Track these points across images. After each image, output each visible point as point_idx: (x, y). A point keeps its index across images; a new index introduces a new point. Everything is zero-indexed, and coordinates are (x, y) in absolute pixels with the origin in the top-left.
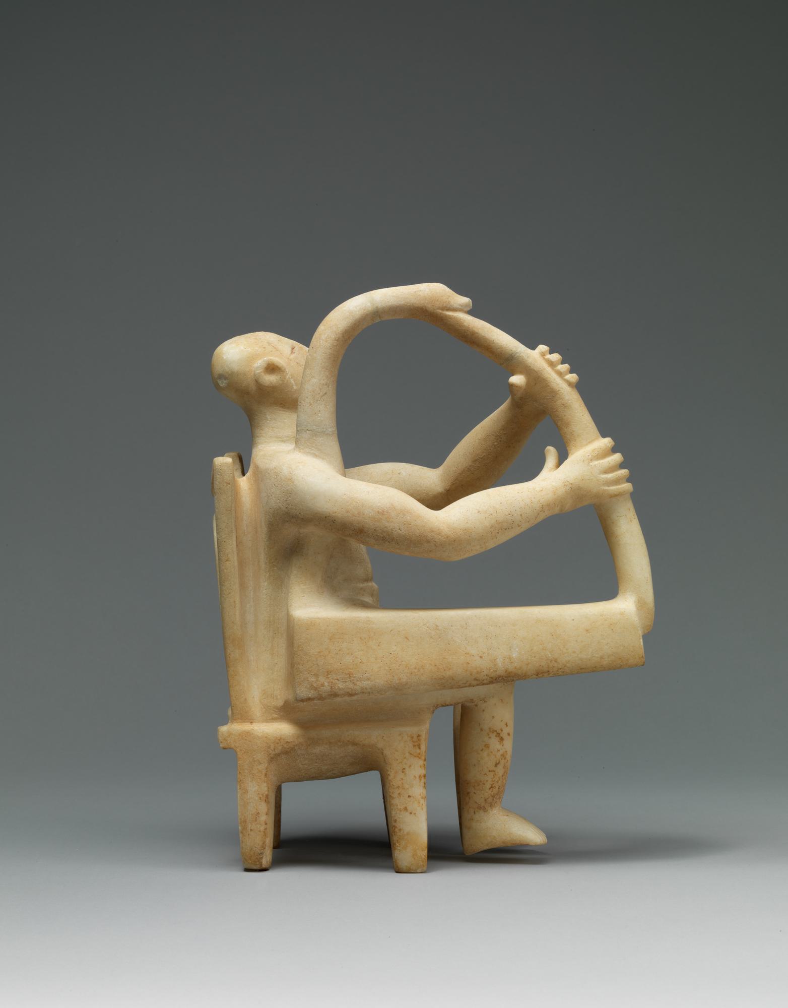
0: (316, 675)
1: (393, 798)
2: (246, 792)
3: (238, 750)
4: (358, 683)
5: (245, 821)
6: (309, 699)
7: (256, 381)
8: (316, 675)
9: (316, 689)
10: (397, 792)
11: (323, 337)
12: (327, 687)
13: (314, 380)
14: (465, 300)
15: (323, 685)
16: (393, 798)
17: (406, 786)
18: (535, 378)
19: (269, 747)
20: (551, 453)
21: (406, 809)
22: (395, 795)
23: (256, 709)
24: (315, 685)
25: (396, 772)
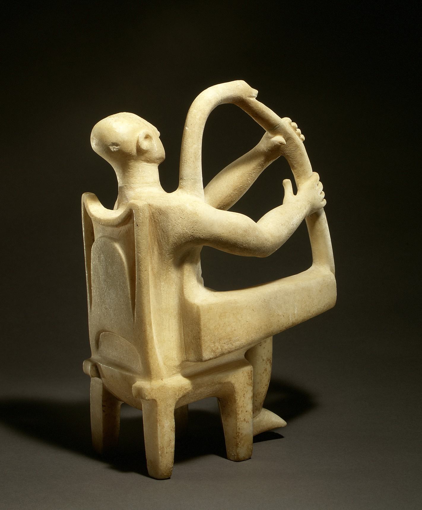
0: (214, 343)
1: (239, 414)
2: (164, 427)
3: (157, 400)
4: (234, 344)
5: (163, 447)
6: (210, 359)
7: (138, 142)
8: (214, 343)
9: (214, 352)
10: (241, 409)
11: (198, 117)
12: (219, 351)
13: (195, 146)
14: (255, 92)
15: (218, 348)
16: (239, 414)
17: (245, 405)
18: (288, 138)
19: (176, 394)
20: (287, 184)
21: (245, 420)
22: (240, 412)
23: (164, 370)
24: (214, 349)
25: (241, 398)
